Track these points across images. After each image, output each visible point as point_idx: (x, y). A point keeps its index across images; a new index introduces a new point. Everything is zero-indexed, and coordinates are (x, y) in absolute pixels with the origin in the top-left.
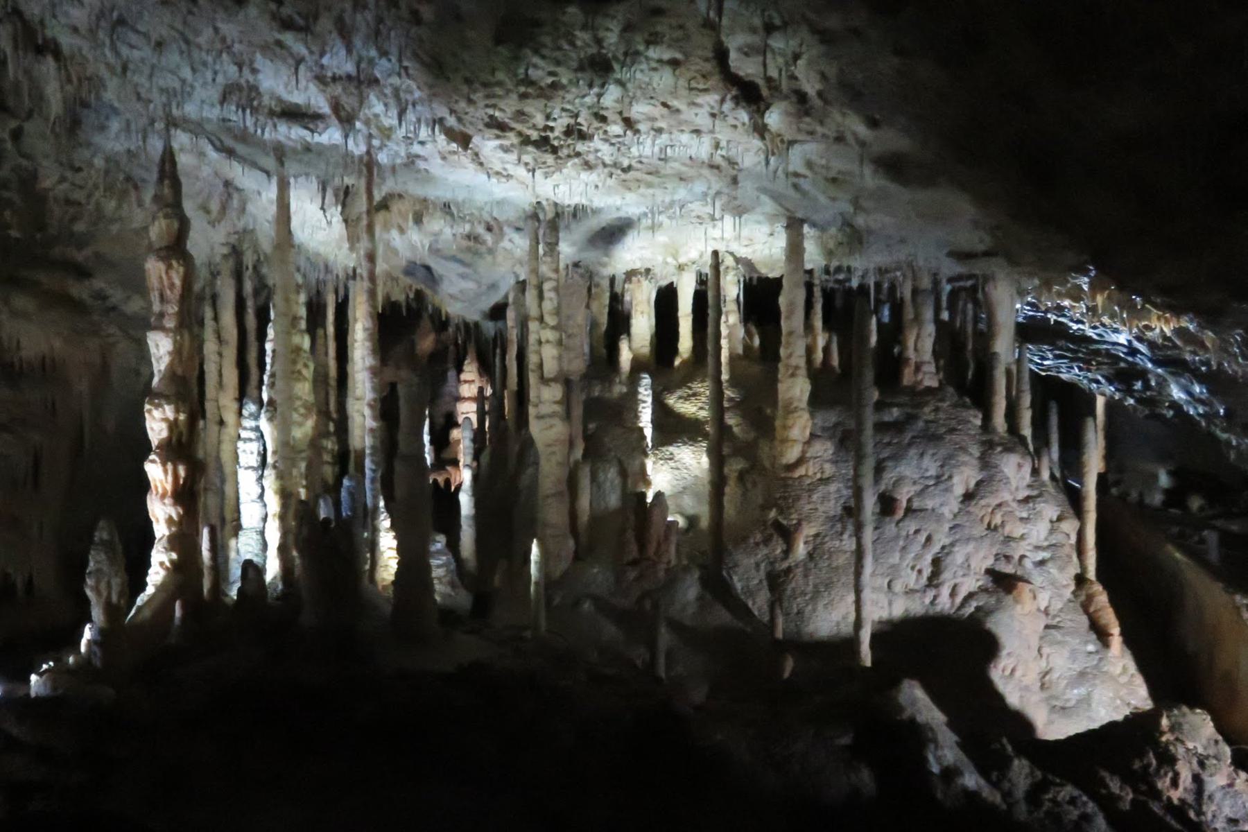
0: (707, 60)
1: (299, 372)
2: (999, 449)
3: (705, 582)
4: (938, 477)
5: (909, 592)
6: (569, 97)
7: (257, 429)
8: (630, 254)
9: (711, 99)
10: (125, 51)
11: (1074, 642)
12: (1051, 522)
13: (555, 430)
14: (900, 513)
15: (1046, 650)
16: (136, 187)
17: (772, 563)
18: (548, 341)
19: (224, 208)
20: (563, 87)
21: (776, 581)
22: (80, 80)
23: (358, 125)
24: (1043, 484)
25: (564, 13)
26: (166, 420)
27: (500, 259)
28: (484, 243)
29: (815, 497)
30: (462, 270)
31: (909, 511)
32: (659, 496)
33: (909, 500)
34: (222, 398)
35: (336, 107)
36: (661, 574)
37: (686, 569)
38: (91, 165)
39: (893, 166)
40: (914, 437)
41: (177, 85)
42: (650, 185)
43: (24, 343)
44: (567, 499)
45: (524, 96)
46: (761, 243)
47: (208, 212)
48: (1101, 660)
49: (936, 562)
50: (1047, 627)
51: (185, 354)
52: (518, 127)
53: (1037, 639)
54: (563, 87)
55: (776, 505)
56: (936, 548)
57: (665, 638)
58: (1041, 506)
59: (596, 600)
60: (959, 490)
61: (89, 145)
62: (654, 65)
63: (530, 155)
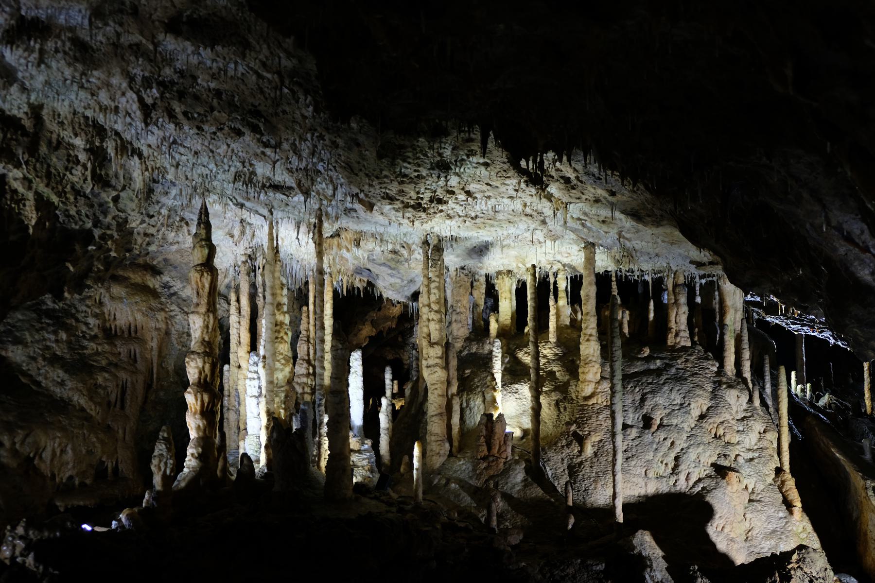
0: (504, 163)
1: (282, 338)
2: (724, 386)
3: (527, 470)
4: (681, 404)
5: (659, 477)
6: (428, 182)
7: (257, 372)
8: (493, 263)
9: (514, 181)
10: (177, 156)
11: (771, 511)
12: (760, 433)
13: (437, 374)
14: (655, 427)
15: (748, 516)
16: (187, 224)
17: (571, 459)
18: (433, 320)
19: (243, 233)
20: (424, 178)
21: (573, 470)
22: (153, 170)
23: (313, 194)
24: (755, 409)
25: (418, 141)
26: (197, 367)
27: (413, 265)
28: (402, 255)
29: (601, 417)
30: (390, 271)
31: (661, 426)
32: (501, 416)
33: (661, 419)
34: (239, 351)
35: (299, 185)
36: (501, 465)
37: (517, 462)
38: (159, 213)
39: (635, 215)
40: (667, 379)
41: (208, 172)
42: (492, 226)
43: (118, 316)
44: (445, 418)
45: (402, 183)
46: (575, 256)
47: (232, 236)
48: (787, 523)
49: (677, 458)
50: (750, 501)
51: (210, 327)
52: (401, 198)
53: (743, 508)
54: (424, 178)
55: (575, 422)
56: (677, 449)
57: (499, 504)
58: (751, 423)
59: (460, 481)
60: (696, 413)
61: (158, 202)
62: (474, 165)
63: (410, 213)
